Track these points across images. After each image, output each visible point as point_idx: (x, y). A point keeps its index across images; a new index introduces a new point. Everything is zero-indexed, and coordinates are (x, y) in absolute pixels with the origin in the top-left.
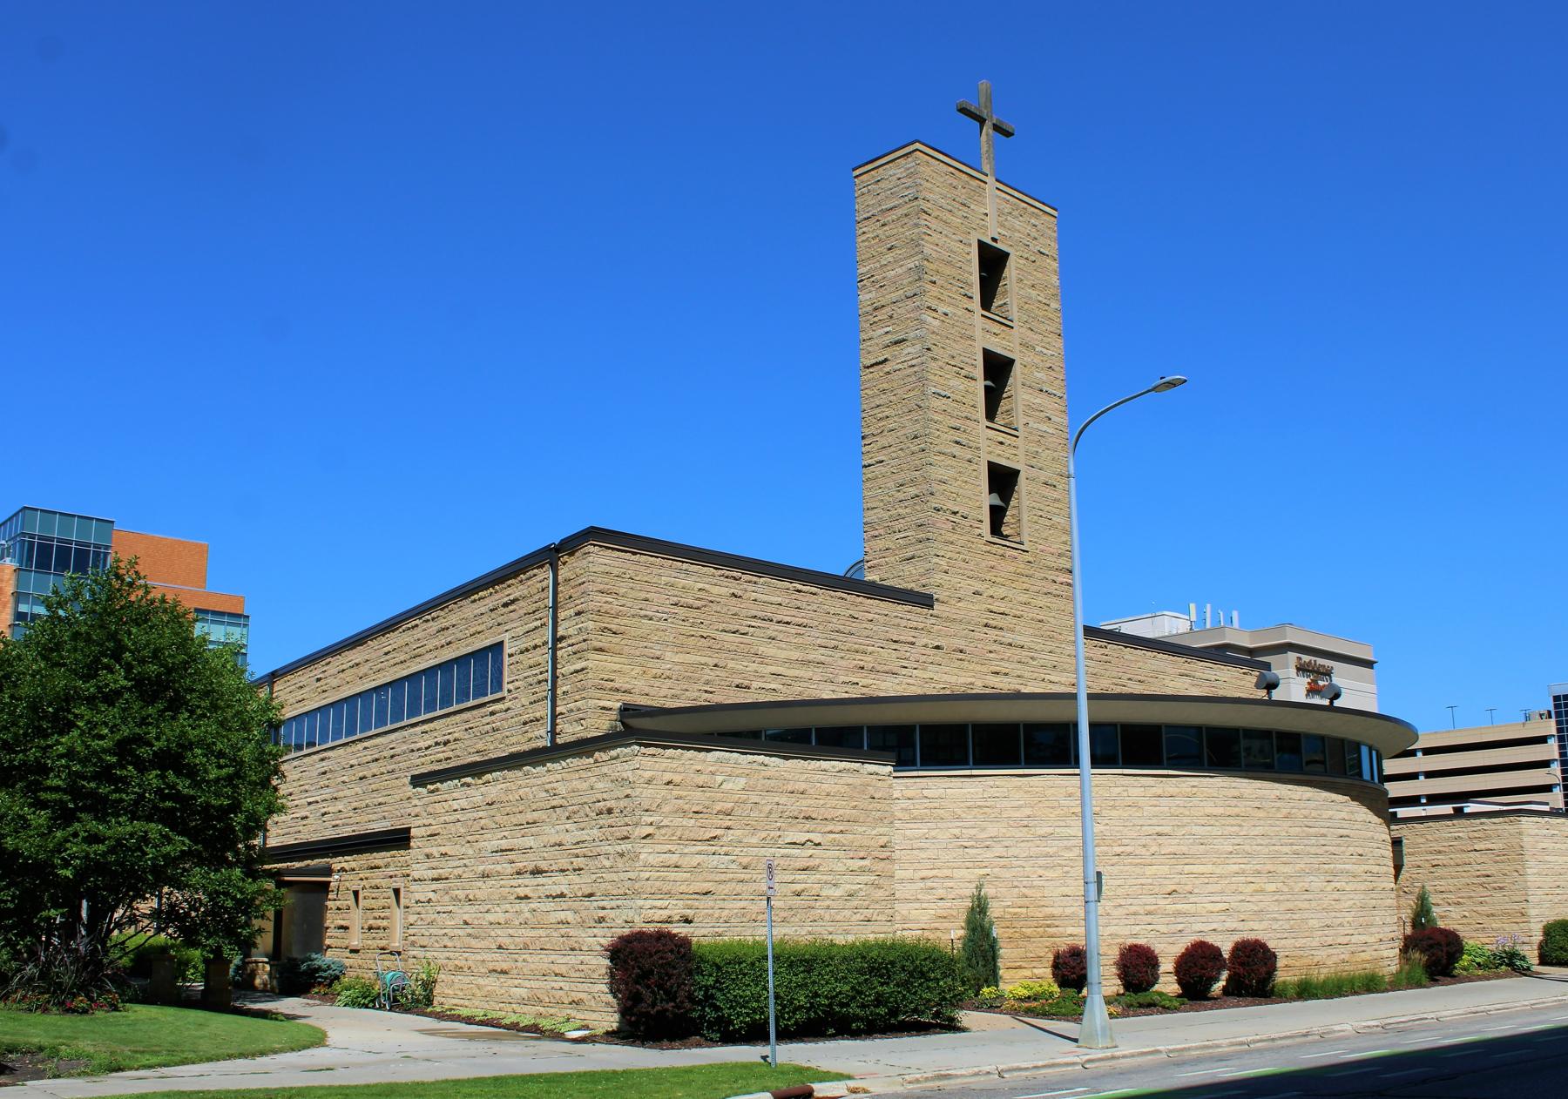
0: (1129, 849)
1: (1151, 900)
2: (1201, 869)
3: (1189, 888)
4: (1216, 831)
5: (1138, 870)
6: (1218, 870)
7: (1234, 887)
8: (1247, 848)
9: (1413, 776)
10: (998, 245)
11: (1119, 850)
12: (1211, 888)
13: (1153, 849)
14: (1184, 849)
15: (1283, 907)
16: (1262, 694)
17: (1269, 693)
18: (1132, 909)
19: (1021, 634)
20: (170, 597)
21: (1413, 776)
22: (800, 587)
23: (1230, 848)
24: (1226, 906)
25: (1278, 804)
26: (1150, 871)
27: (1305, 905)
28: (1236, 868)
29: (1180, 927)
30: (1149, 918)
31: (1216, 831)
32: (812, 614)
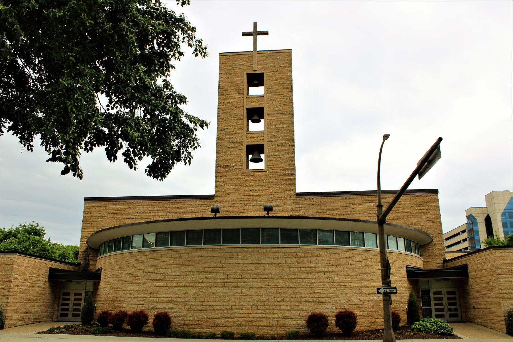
0: (139, 278)
1: (144, 296)
2: (162, 284)
3: (157, 292)
4: (169, 270)
5: (142, 285)
6: (169, 285)
7: (174, 292)
8: (182, 277)
9: (459, 242)
10: (264, 44)
11: (137, 278)
12: (165, 292)
13: (147, 277)
14: (157, 277)
15: (198, 300)
16: (213, 215)
17: (215, 214)
18: (139, 299)
19: (260, 201)
20: (45, 232)
21: (459, 242)
22: (154, 201)
23: (174, 277)
24: (170, 299)
25: (201, 259)
26: (145, 285)
27: (214, 300)
28: (176, 284)
29: (152, 306)
30: (143, 302)
31: (169, 270)
32: (160, 209)
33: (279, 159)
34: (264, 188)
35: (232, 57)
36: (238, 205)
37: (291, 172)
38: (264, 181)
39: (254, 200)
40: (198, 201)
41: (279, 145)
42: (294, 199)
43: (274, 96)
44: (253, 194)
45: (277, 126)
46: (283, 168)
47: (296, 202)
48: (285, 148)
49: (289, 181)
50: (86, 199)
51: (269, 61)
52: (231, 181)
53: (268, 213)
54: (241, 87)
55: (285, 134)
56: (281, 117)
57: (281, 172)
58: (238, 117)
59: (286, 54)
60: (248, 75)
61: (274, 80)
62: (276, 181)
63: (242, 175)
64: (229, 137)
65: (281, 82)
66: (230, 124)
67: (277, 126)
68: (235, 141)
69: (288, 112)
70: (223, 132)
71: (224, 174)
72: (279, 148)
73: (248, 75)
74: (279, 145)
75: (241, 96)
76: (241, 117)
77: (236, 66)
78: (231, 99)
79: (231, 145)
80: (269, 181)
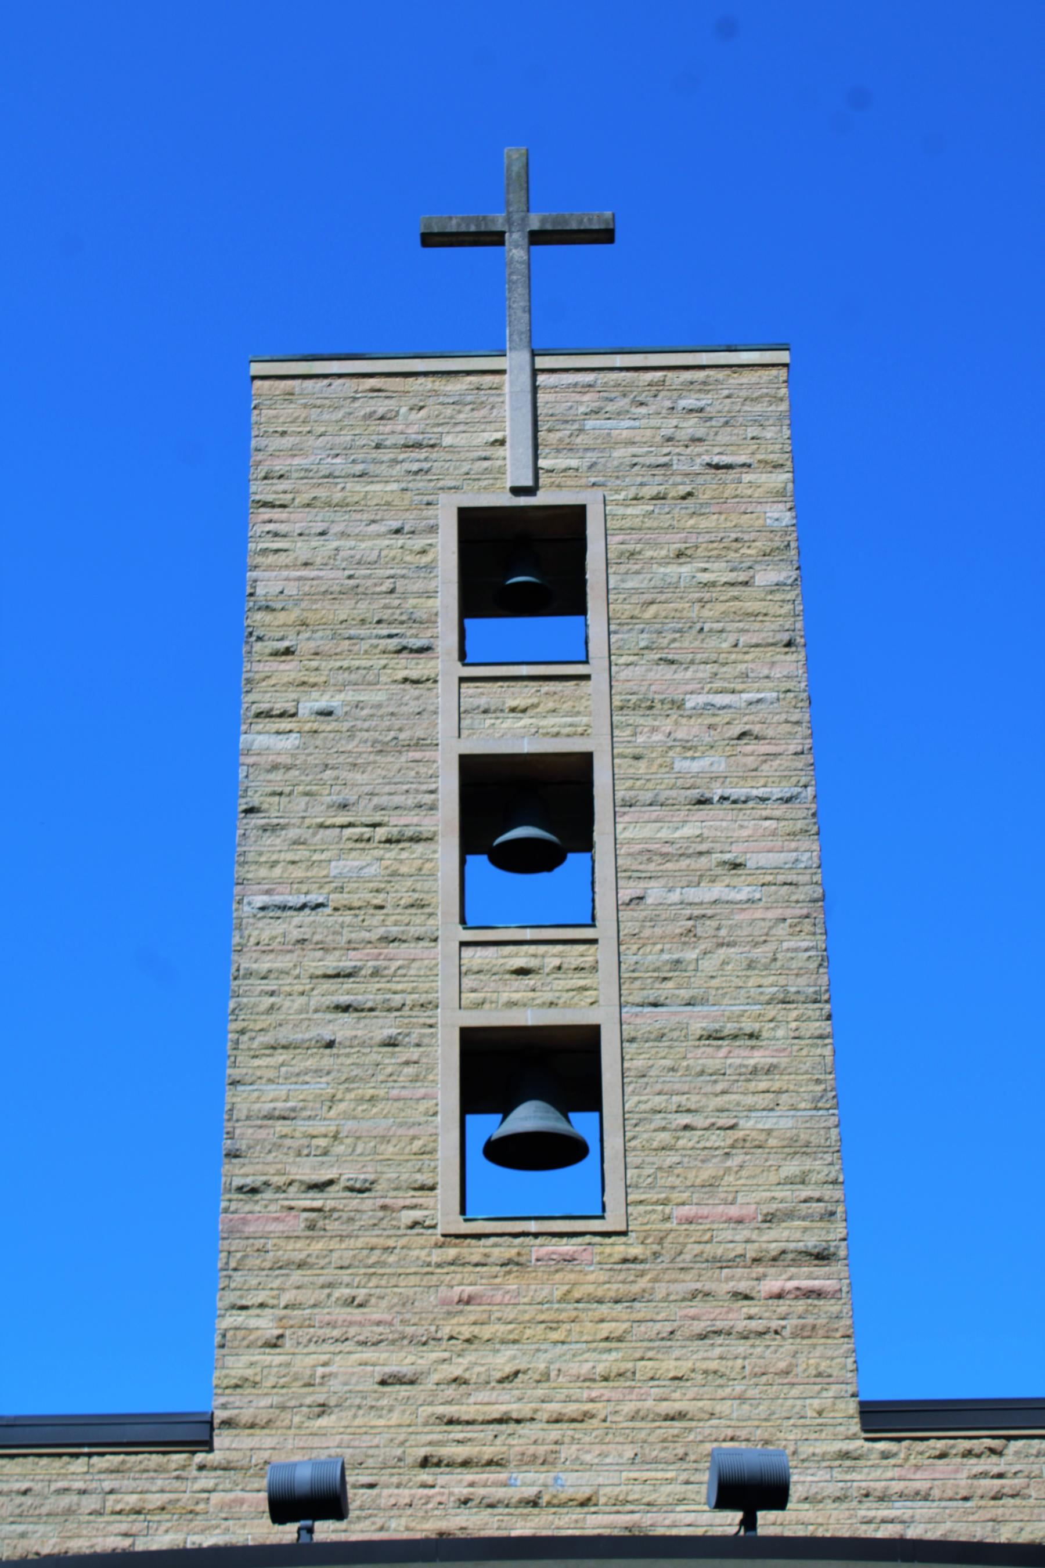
19: (580, 1465)
33: (715, 1139)
34: (608, 1361)
35: (351, 384)
36: (405, 1495)
37: (811, 1242)
38: (604, 1310)
39: (529, 1461)
40: (79, 1465)
41: (713, 1037)
42: (846, 1455)
43: (666, 672)
44: (515, 1409)
45: (693, 894)
46: (748, 1204)
47: (862, 1478)
48: (759, 1058)
49: (801, 1305)
50: (505, 355)
51: (622, 429)
52: (351, 1302)
53: (749, 1522)
54: (424, 607)
55: (760, 953)
56: (713, 823)
57: (733, 1241)
58: (397, 823)
59: (748, 377)
60: (471, 521)
61: (665, 562)
62: (697, 1308)
63: (436, 1256)
64: (332, 963)
65: (718, 572)
66: (335, 868)
67: (693, 894)
68: (369, 999)
69: (776, 792)
70: (279, 928)
71: (296, 1250)
72: (714, 1057)
73: (471, 521)
74: (713, 1037)
75: (418, 668)
76: (426, 824)
77: (386, 455)
78: (342, 687)
79: (342, 1027)
80: (641, 1310)
